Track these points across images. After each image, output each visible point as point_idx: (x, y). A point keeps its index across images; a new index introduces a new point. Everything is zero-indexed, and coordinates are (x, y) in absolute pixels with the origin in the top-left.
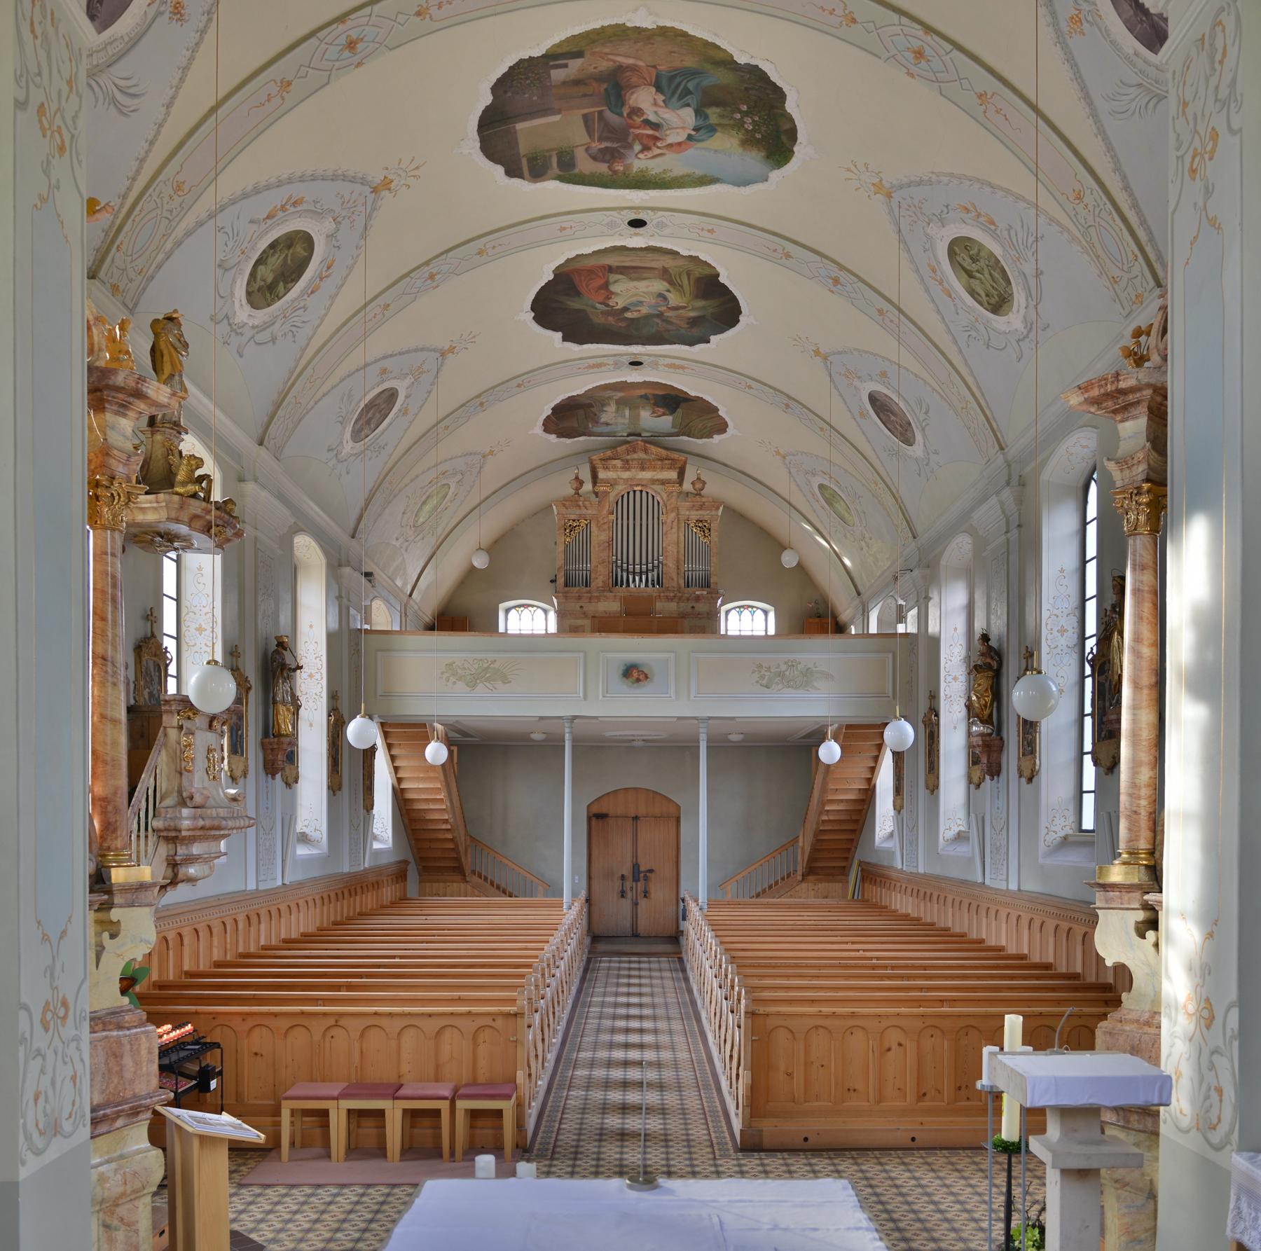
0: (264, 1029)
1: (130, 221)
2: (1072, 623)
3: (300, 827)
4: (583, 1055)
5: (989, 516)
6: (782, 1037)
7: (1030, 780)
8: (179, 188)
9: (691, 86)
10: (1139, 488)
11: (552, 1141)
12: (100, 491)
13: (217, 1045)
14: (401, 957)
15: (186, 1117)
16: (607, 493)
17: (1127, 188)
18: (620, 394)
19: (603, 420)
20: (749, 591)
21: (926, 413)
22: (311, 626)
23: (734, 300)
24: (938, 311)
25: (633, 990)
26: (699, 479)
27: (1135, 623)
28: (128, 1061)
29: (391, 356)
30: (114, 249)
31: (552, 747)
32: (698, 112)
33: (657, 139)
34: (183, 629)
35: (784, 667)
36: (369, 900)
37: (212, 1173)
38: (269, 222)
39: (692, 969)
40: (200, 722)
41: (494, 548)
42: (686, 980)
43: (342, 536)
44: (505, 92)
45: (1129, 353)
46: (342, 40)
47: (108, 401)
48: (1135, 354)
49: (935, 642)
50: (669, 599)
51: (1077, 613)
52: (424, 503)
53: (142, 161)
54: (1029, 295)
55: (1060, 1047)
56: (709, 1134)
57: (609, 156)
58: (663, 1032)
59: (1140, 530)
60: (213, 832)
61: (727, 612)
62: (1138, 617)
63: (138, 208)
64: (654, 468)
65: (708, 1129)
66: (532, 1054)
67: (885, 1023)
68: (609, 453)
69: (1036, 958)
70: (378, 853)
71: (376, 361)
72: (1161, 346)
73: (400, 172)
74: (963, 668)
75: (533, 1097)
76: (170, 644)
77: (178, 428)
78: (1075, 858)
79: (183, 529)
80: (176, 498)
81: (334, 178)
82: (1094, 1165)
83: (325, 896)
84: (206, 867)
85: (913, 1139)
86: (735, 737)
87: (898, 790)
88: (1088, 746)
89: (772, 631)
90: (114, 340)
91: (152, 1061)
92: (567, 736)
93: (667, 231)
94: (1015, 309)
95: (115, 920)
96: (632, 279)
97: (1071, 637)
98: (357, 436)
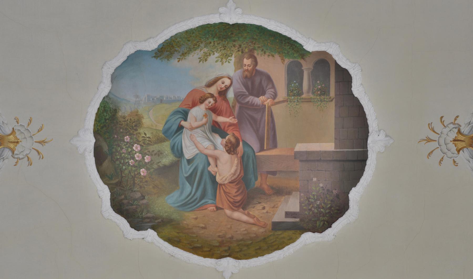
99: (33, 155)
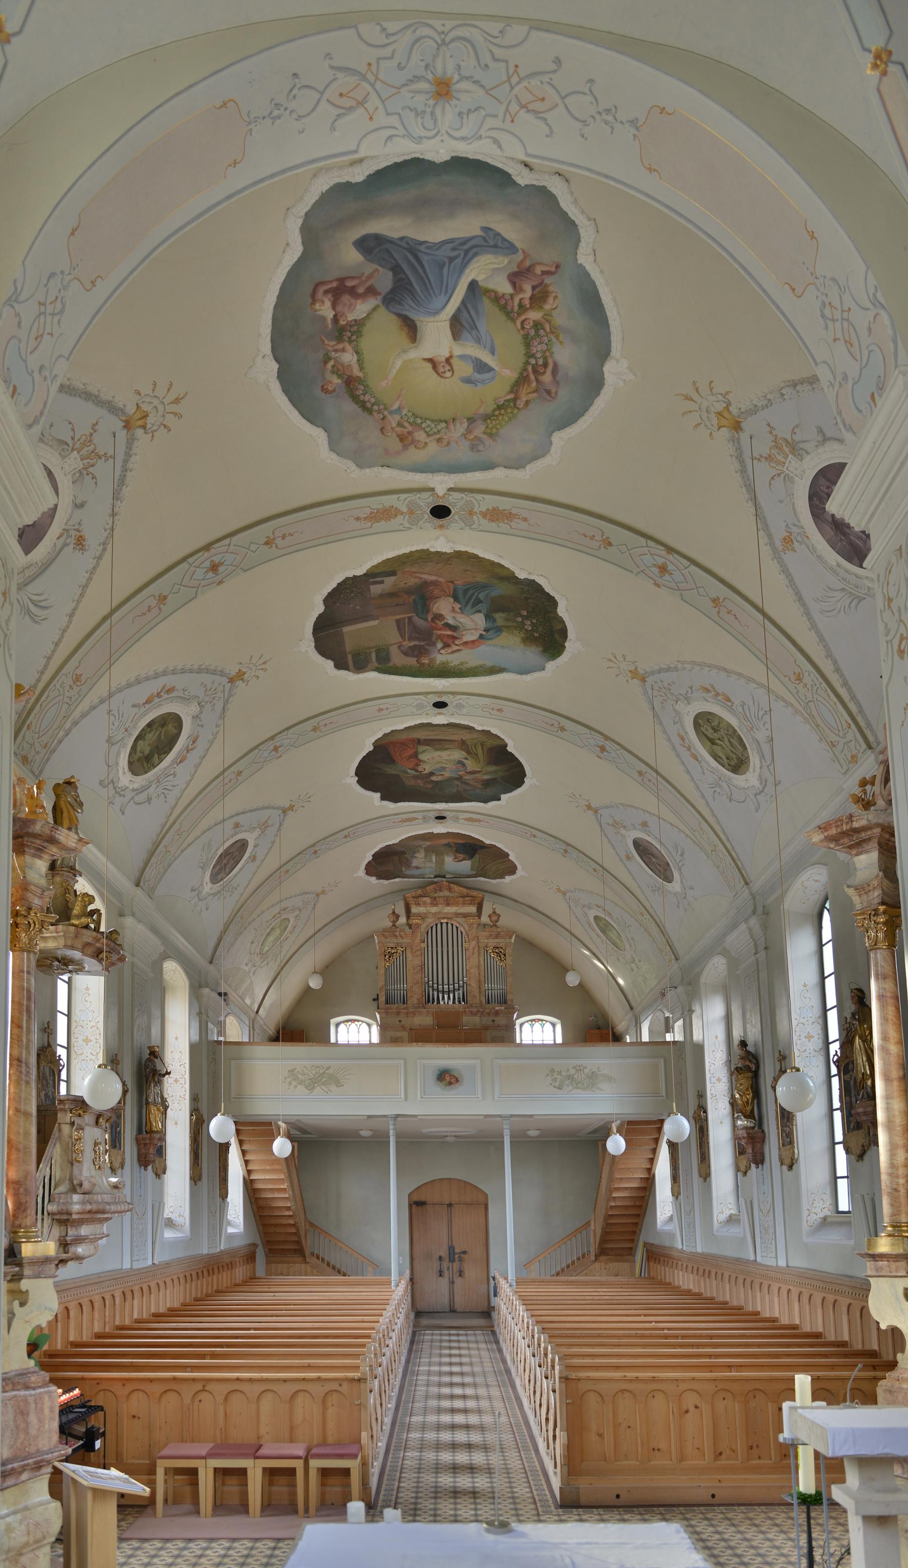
0: (141, 1394)
1: (38, 706)
2: (817, 1030)
3: (167, 1213)
4: (414, 1419)
5: (739, 939)
6: (592, 1401)
7: (790, 1167)
8: (77, 679)
9: (481, 596)
10: (876, 910)
11: (394, 1498)
12: (19, 920)
13: (101, 1408)
14: (255, 1329)
15: (82, 1474)
16: (418, 925)
17: (838, 670)
18: (428, 843)
19: (413, 865)
20: (541, 1006)
21: (682, 855)
22: (177, 1038)
23: (520, 765)
24: (688, 772)
25: (454, 1360)
26: (494, 912)
27: (881, 1024)
28: (33, 1418)
29: (243, 813)
30: (25, 727)
31: (379, 1141)
32: (488, 617)
33: (455, 638)
34: (73, 1040)
35: (572, 1071)
36: (224, 1279)
37: (103, 1522)
38: (147, 706)
39: (505, 1341)
40: (89, 1118)
41: (325, 971)
42: (500, 1350)
43: (200, 960)
44: (335, 603)
45: (858, 800)
46: (207, 564)
47: (28, 846)
48: (863, 800)
49: (699, 1049)
50: (473, 1014)
51: (821, 1021)
52: (269, 934)
53: (49, 658)
54: (762, 757)
55: (852, 1401)
56: (532, 1492)
57: (418, 652)
58: (483, 1398)
59: (880, 945)
60: (99, 1216)
61: (521, 1025)
62: (884, 1019)
63: (46, 694)
64: (457, 904)
65: (530, 1487)
66: (374, 1417)
67: (683, 1386)
68: (419, 892)
69: (807, 1328)
70: (232, 1236)
71: (230, 817)
72: (885, 793)
73: (251, 666)
74: (726, 1071)
75: (375, 1458)
76: (62, 1052)
77: (74, 872)
78: (834, 1237)
79: (77, 955)
80: (72, 929)
81: (199, 671)
82: (893, 1512)
83: (188, 1275)
84: (91, 1247)
85: (713, 1496)
86: (533, 1133)
87: (675, 1178)
88: (839, 1137)
89: (559, 1040)
90: (32, 797)
91: (52, 1419)
92: (391, 1132)
93: (464, 711)
94: (751, 769)
95: (24, 1290)
96: (437, 750)
97: (818, 1042)
98: (214, 879)
99: (170, 420)
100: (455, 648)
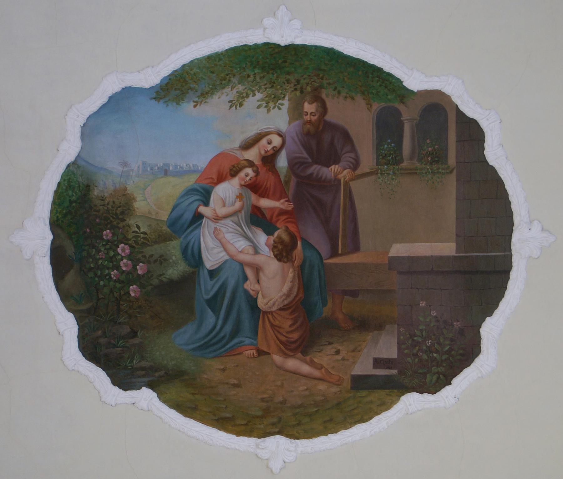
32: (194, 258)
100: (252, 155)
